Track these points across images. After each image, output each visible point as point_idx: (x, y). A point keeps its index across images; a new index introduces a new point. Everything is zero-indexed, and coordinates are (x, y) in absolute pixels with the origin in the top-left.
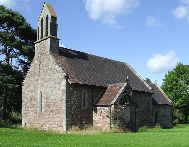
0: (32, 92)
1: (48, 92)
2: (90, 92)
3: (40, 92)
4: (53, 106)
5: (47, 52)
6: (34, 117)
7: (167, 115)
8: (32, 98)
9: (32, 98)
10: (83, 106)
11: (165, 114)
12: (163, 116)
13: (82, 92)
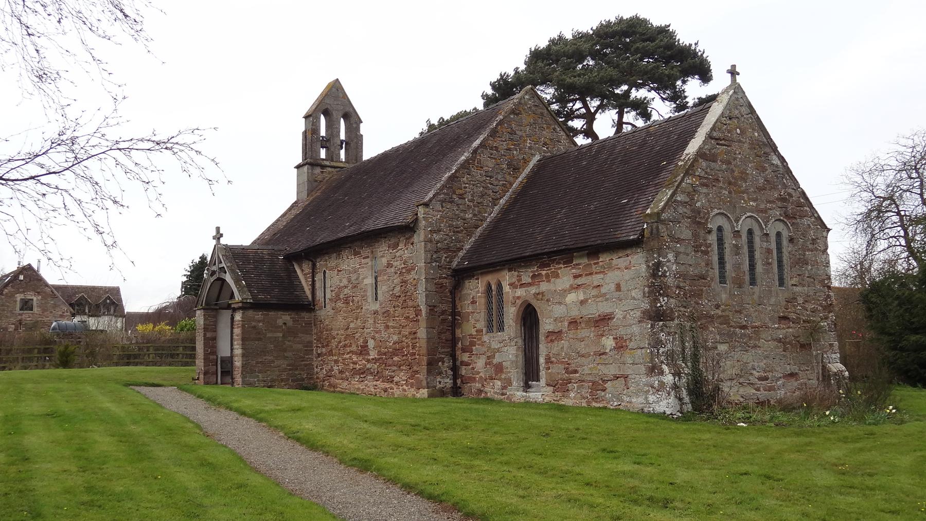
11: (596, 309)
12: (574, 323)
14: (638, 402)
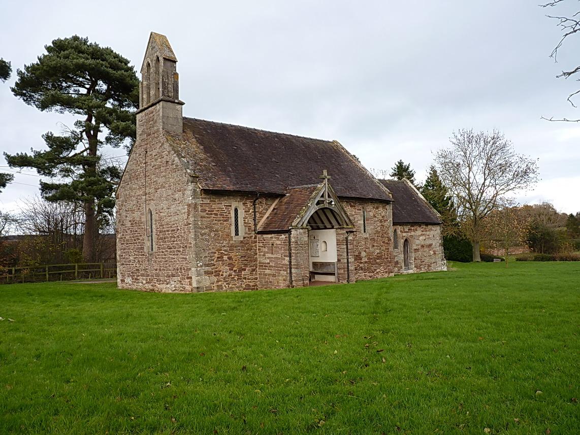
0: (133, 211)
1: (163, 209)
2: (249, 204)
3: (147, 209)
4: (171, 237)
5: (158, 131)
6: (139, 261)
8: (133, 222)
9: (133, 222)
10: (233, 234)
11: (428, 242)
12: (423, 246)
13: (231, 206)
14: (439, 269)
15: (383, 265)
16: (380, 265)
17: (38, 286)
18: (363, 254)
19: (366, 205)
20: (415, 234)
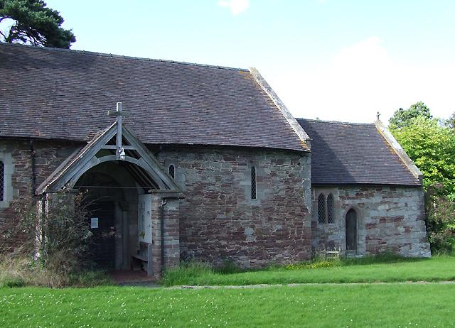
7: (402, 218)
11: (393, 214)
12: (383, 220)
15: (289, 247)
16: (283, 247)
17: (389, 269)
18: (249, 231)
19: (257, 157)
20: (370, 201)
